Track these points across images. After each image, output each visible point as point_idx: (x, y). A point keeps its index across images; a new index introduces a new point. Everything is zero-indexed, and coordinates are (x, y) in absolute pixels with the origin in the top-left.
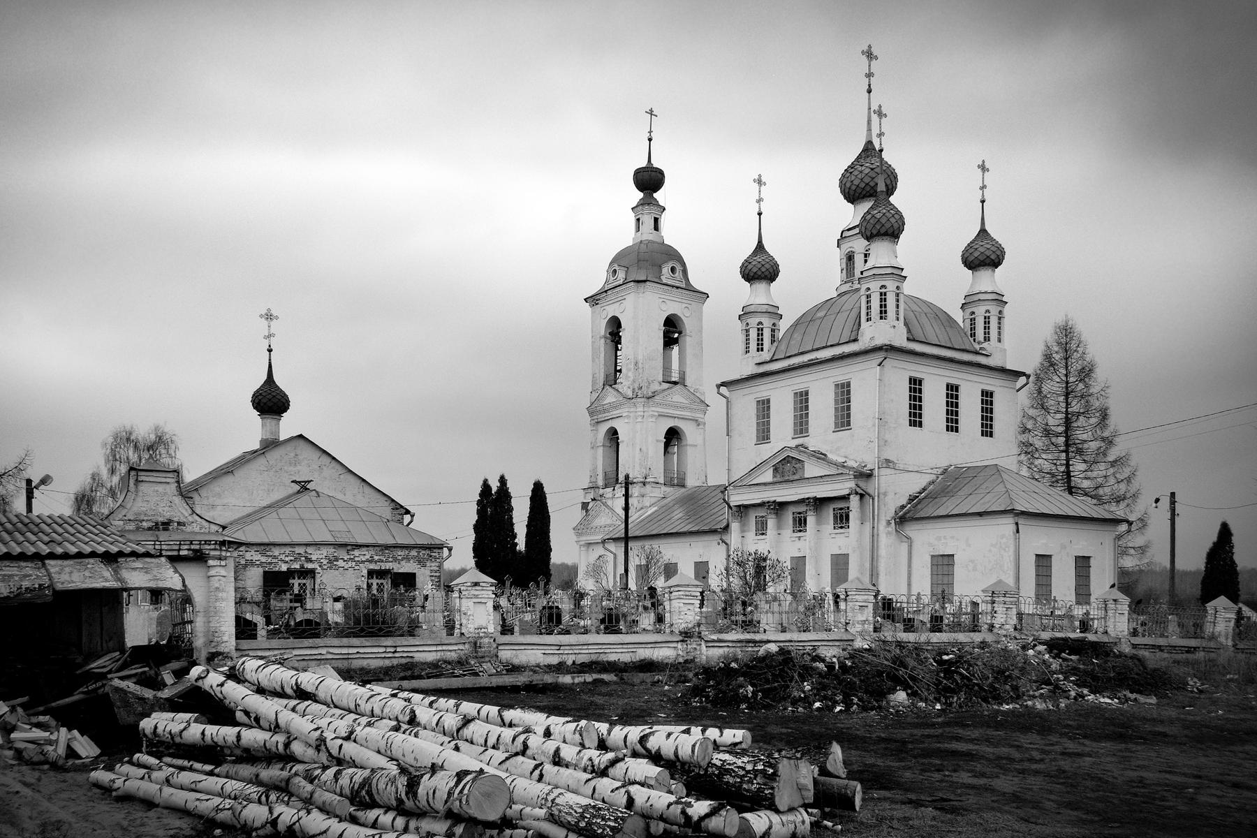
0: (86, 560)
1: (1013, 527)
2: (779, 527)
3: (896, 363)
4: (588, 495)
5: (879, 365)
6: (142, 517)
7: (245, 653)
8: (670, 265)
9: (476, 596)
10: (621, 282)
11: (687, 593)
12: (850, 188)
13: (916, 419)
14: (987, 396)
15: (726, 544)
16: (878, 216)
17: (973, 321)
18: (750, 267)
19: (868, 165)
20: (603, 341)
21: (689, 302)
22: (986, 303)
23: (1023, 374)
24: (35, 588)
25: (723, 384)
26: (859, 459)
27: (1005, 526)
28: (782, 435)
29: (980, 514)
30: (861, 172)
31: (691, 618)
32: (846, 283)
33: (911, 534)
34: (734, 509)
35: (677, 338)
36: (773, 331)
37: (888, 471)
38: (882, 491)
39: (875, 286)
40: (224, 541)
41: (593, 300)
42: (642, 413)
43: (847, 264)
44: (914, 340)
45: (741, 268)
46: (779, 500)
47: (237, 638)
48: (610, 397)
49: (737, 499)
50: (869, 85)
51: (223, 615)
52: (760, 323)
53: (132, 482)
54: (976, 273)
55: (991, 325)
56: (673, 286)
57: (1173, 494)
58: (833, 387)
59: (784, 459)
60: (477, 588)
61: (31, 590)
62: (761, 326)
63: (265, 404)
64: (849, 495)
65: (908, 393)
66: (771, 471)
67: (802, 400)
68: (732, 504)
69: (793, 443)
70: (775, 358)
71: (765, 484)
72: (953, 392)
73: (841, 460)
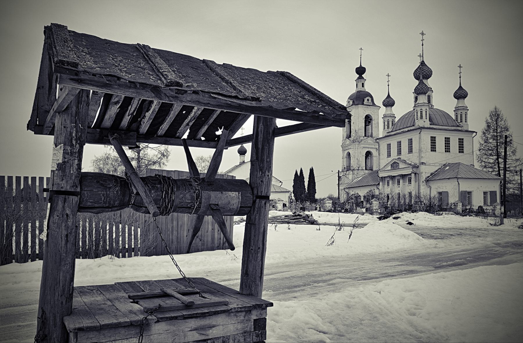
2: (393, 183)
3: (425, 132)
8: (367, 98)
13: (433, 149)
14: (461, 141)
23: (474, 132)
29: (449, 179)
30: (419, 71)
34: (380, 178)
38: (421, 172)
44: (434, 124)
46: (392, 175)
49: (381, 175)
52: (426, 109)
58: (386, 145)
66: (390, 166)
67: (399, 143)
69: (397, 157)
71: (388, 170)
72: (447, 140)
73: (410, 163)
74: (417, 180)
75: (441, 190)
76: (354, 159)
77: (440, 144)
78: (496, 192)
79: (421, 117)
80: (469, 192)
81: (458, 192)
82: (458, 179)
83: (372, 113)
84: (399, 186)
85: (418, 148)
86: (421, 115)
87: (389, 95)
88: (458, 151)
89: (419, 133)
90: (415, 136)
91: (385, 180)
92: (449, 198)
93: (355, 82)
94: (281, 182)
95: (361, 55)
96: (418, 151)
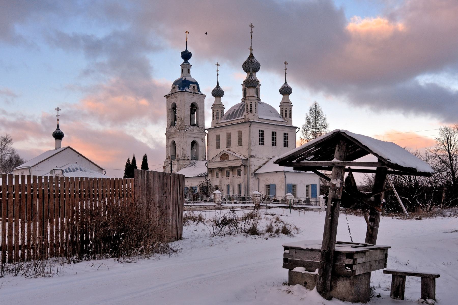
2: (222, 175)
4: (165, 163)
12: (245, 69)
13: (262, 142)
14: (286, 136)
20: (170, 111)
21: (200, 98)
22: (286, 106)
23: (297, 128)
28: (223, 147)
38: (250, 165)
41: (167, 96)
46: (222, 167)
48: (173, 129)
50: (252, 36)
52: (256, 103)
55: (287, 113)
59: (223, 154)
64: (241, 166)
66: (220, 158)
68: (209, 168)
72: (274, 134)
75: (269, 183)
76: (179, 148)
77: (268, 138)
78: (316, 185)
80: (294, 185)
81: (285, 185)
82: (285, 173)
83: (198, 101)
84: (228, 178)
85: (247, 141)
86: (251, 108)
88: (271, 144)
89: (249, 127)
90: (245, 129)
91: (213, 171)
92: (276, 190)
93: (181, 67)
96: (247, 144)
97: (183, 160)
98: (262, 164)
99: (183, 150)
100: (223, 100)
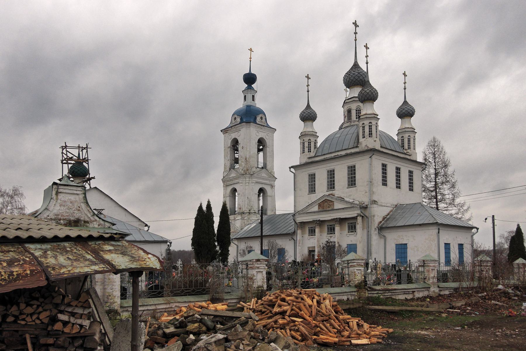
0: (62, 244)
1: (437, 231)
2: (321, 232)
5: (370, 158)
6: (60, 217)
7: (125, 309)
9: (258, 268)
10: (238, 123)
11: (359, 264)
12: (349, 81)
14: (411, 172)
15: (294, 240)
16: (368, 91)
17: (403, 140)
18: (304, 115)
19: (357, 71)
20: (229, 149)
21: (269, 133)
22: (409, 132)
24: (27, 274)
25: (292, 167)
26: (360, 200)
27: (433, 231)
28: (322, 189)
30: (354, 74)
31: (360, 278)
32: (347, 122)
33: (385, 234)
35: (262, 149)
36: (315, 143)
37: (375, 206)
38: (372, 215)
39: (366, 122)
40: (117, 233)
41: (225, 131)
42: (248, 181)
43: (348, 114)
45: (300, 117)
46: (321, 219)
47: (121, 299)
48: (233, 174)
49: (299, 219)
51: (115, 284)
53: (54, 192)
54: (403, 120)
56: (262, 125)
57: (493, 216)
58: (307, 176)
60: (259, 263)
61: (23, 276)
62: (310, 141)
63: (76, 172)
64: (357, 216)
65: (381, 171)
67: (331, 174)
68: (297, 222)
70: (316, 155)
71: (314, 212)
72: (398, 170)
73: (351, 201)
74: (367, 227)
79: (369, 134)
83: (267, 136)
87: (308, 106)
94: (146, 225)
95: (250, 58)
97: (248, 214)
98: (386, 214)
99: (248, 200)
100: (317, 126)
